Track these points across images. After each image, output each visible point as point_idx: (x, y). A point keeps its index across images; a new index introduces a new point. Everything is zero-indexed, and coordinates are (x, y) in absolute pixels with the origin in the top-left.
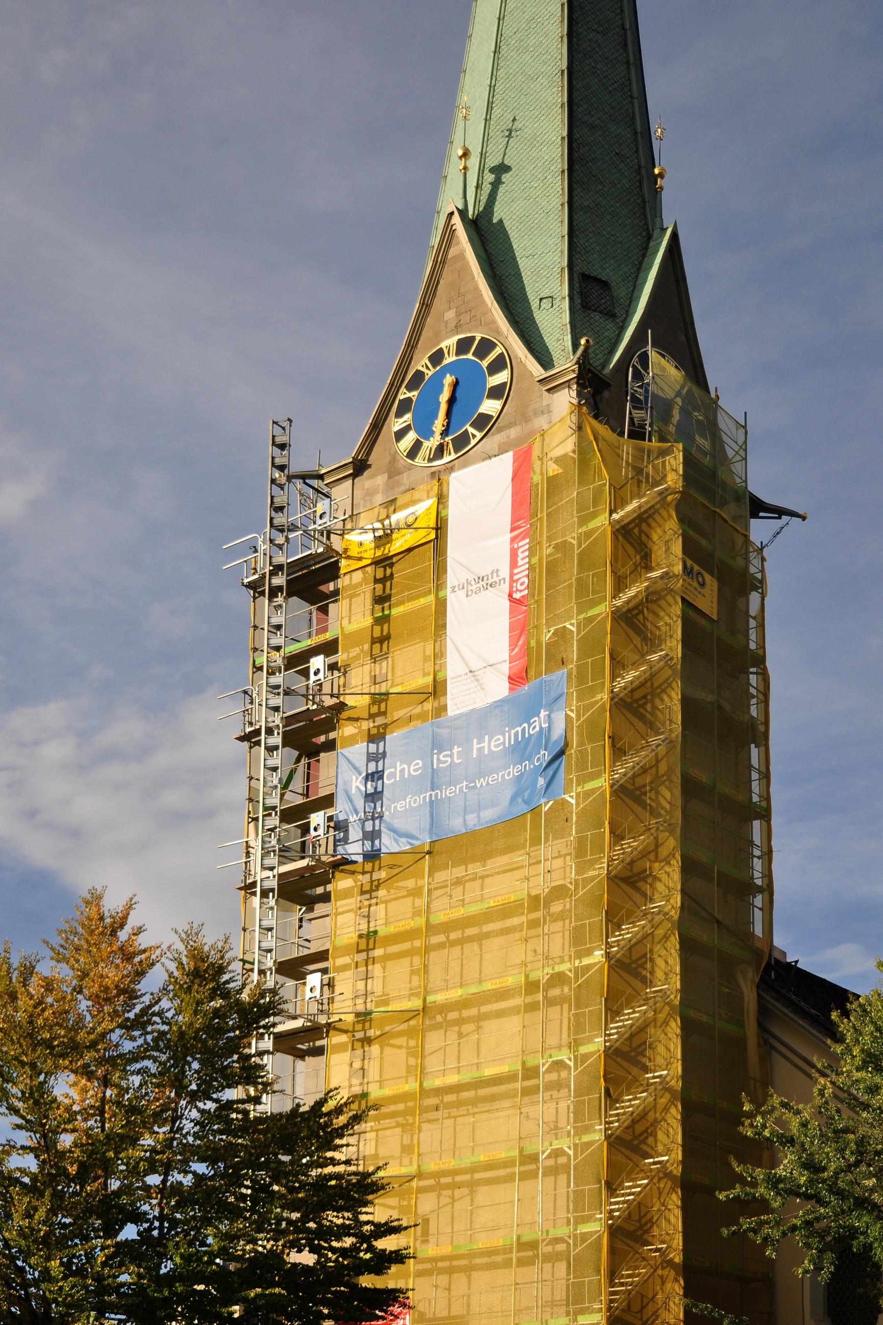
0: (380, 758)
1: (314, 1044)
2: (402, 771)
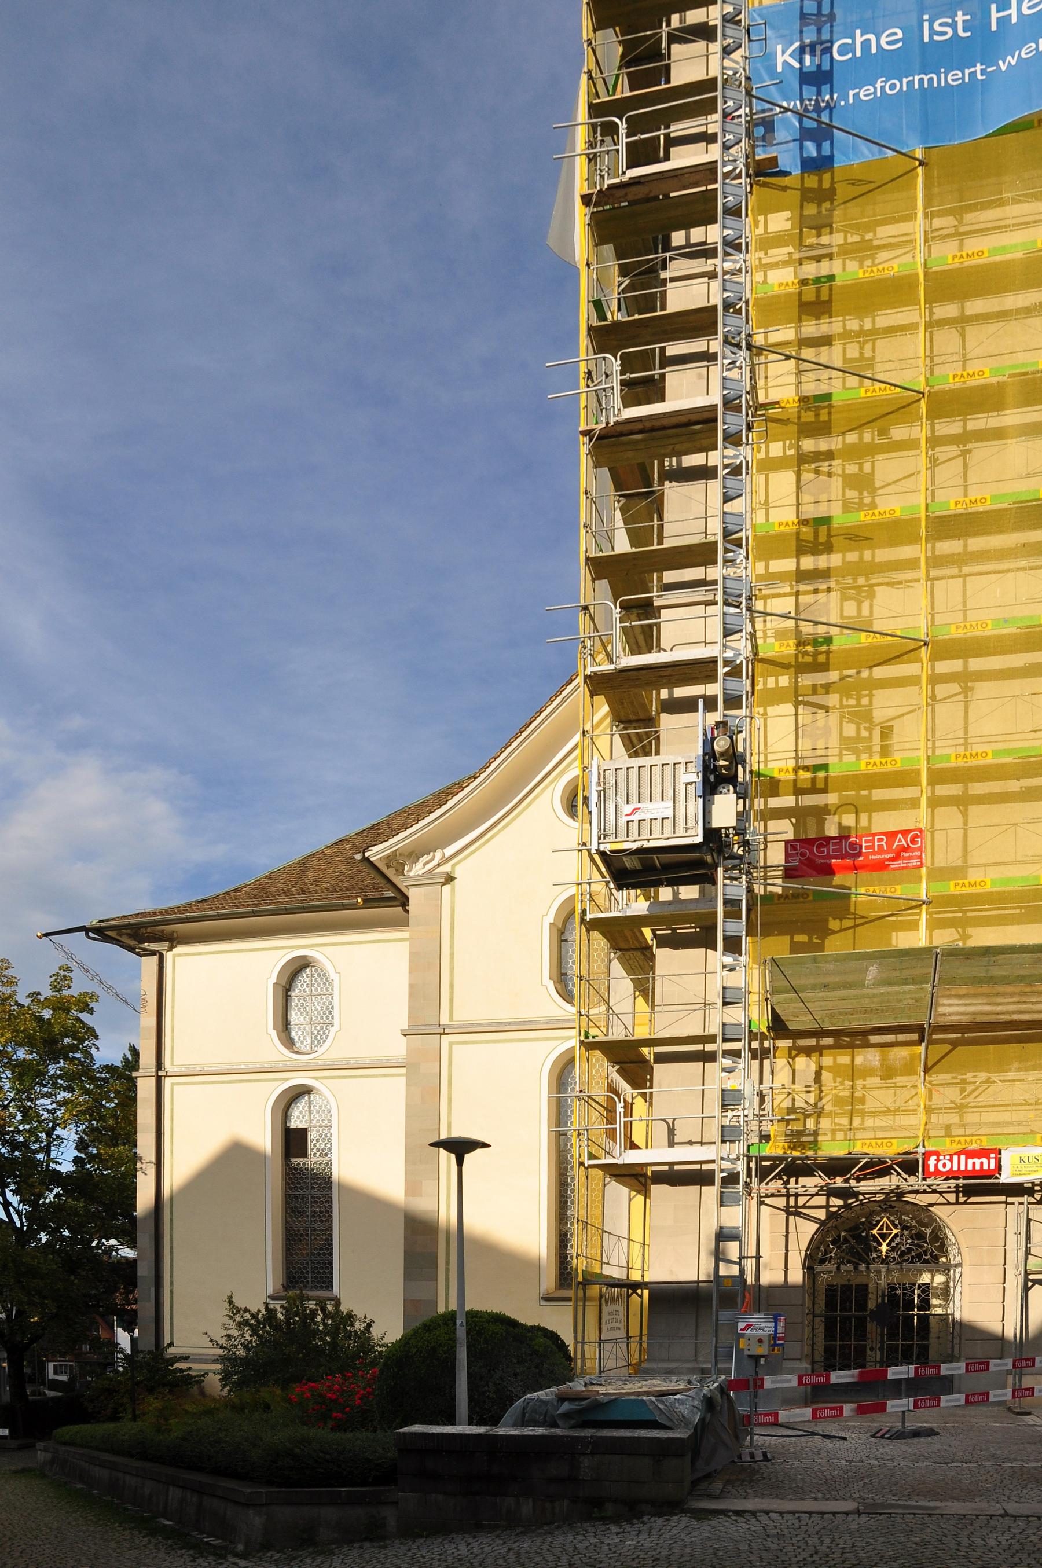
0: (825, 22)
1: (679, 462)
2: (866, 44)
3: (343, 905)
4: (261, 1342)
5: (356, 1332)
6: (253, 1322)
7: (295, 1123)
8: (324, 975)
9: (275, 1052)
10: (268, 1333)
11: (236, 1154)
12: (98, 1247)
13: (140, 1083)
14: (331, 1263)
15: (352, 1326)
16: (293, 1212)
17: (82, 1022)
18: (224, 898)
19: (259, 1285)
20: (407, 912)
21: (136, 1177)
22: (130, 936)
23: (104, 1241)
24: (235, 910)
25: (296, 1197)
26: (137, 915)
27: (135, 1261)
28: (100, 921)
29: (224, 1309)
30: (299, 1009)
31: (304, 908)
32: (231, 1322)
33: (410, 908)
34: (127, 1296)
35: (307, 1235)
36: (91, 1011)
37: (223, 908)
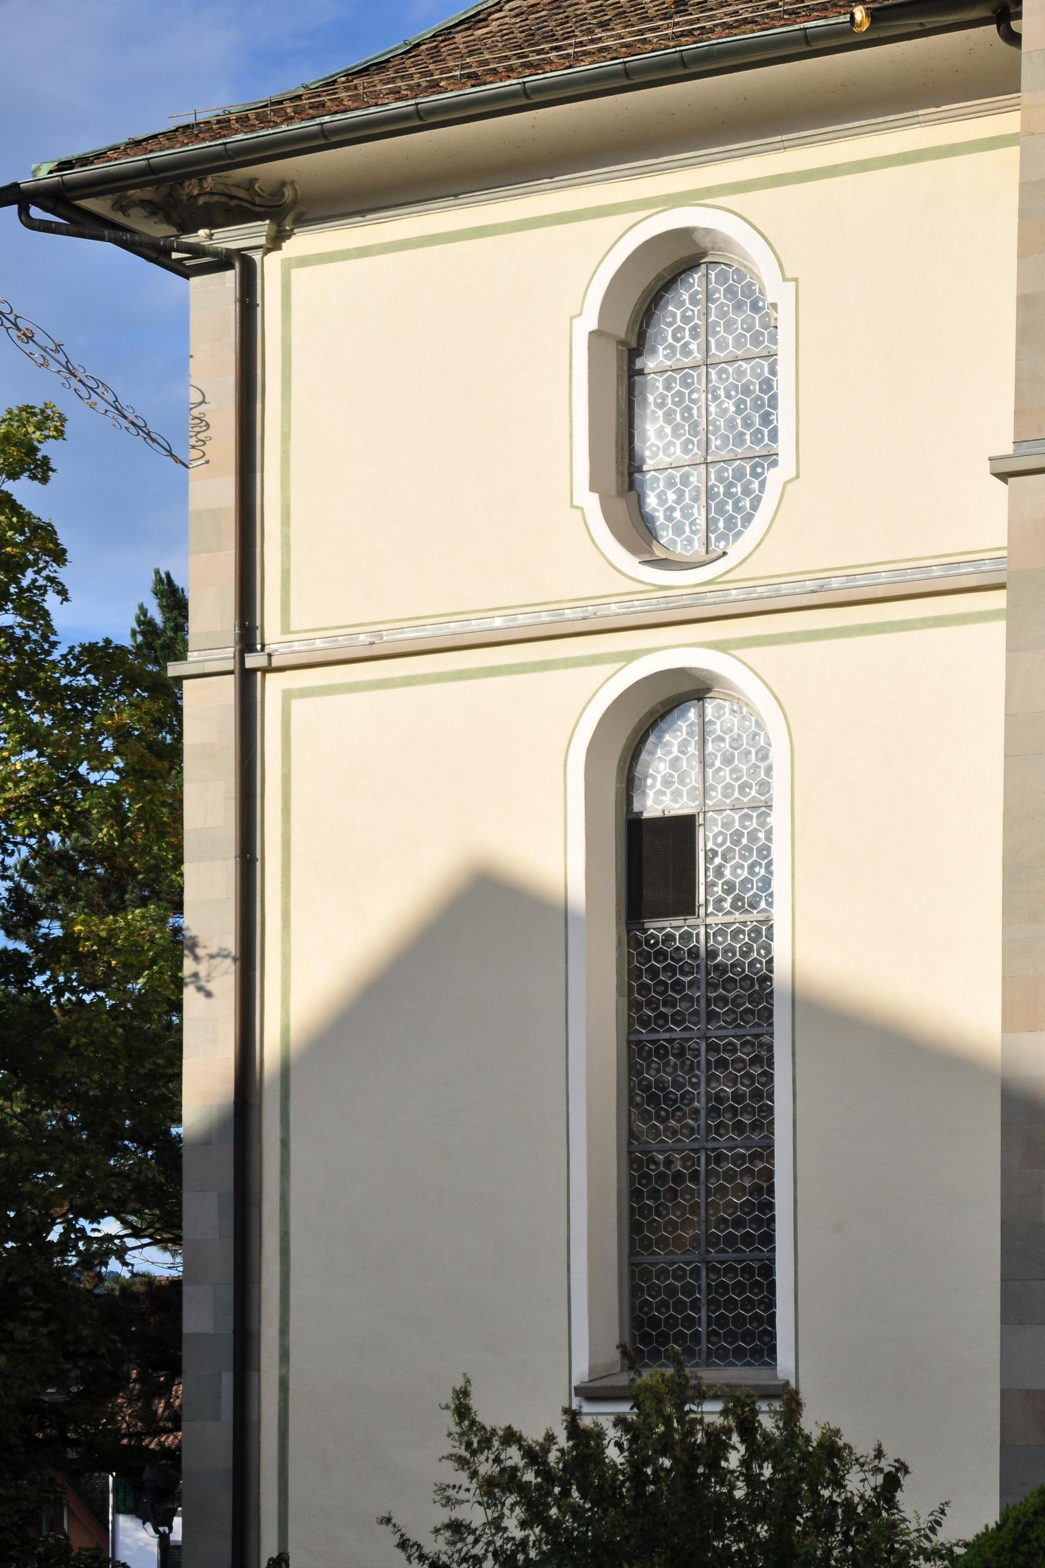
3: (806, 37)
4: (555, 1544)
5: (849, 1505)
6: (529, 1476)
7: (656, 803)
8: (749, 298)
9: (600, 566)
10: (576, 1512)
11: (484, 907)
12: (65, 1245)
13: (191, 694)
14: (768, 1270)
15: (838, 1484)
16: (653, 1099)
17: (15, 508)
18: (435, 54)
19: (550, 1354)
20: (1014, 39)
21: (177, 1007)
22: (154, 209)
23: (82, 1222)
24: (470, 91)
25: (661, 1051)
26: (170, 136)
27: (175, 1285)
28: (65, 165)
29: (441, 1435)
30: (669, 416)
31: (683, 62)
32: (462, 1478)
33: (1027, 25)
34: (148, 1405)
35: (695, 1177)
36: (42, 471)
37: (434, 87)
